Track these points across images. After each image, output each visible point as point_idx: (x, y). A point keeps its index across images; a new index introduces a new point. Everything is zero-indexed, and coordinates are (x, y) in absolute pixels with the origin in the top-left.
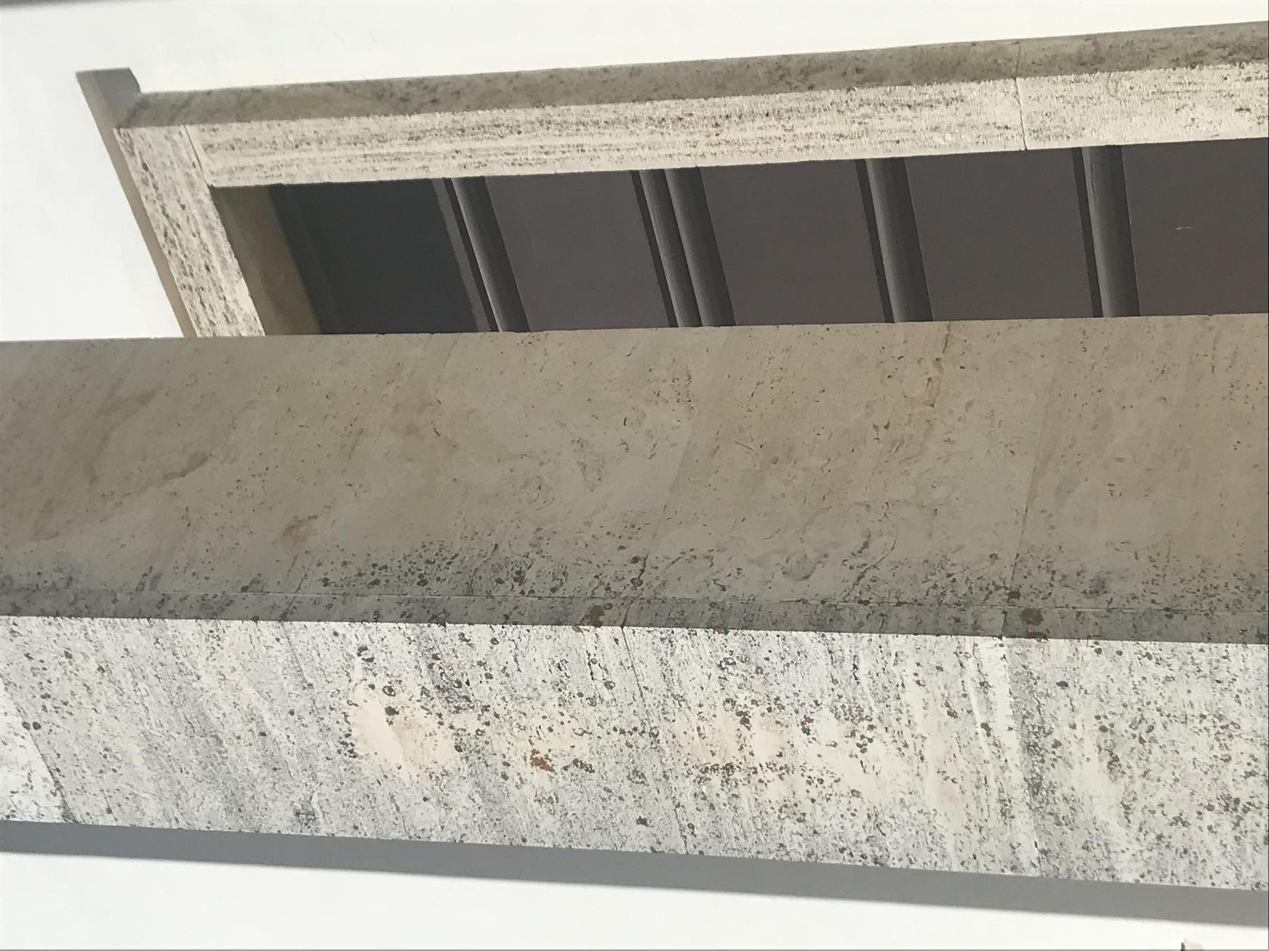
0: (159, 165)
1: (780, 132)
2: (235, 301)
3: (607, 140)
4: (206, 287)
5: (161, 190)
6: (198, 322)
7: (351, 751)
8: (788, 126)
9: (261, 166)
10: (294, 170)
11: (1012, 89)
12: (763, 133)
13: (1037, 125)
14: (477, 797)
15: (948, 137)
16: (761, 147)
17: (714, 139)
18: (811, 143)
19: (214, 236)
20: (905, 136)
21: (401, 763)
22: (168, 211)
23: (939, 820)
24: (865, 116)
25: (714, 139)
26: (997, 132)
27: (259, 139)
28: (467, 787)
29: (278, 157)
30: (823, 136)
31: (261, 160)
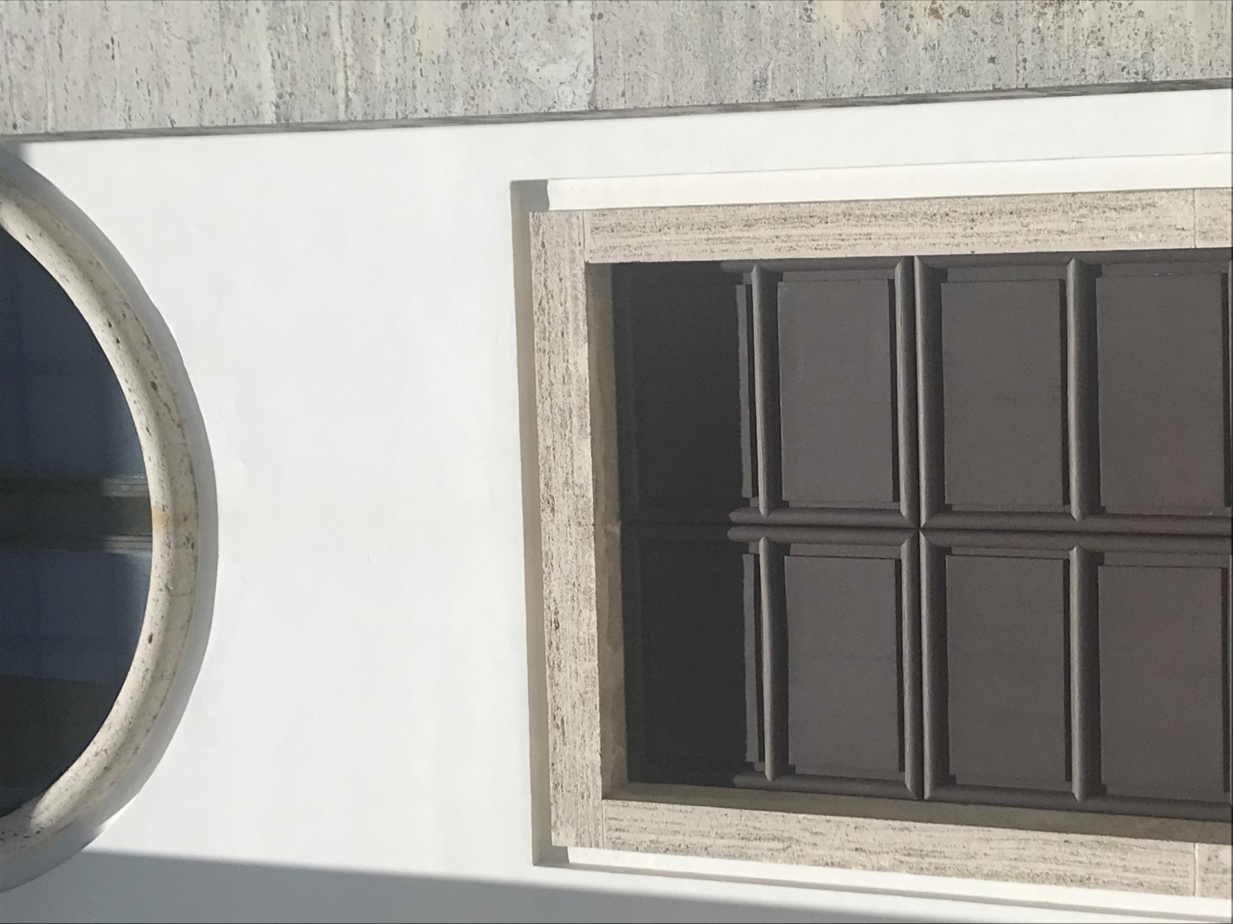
0: (554, 243)
1: (1018, 228)
2: (575, 363)
3: (890, 230)
4: (556, 351)
5: (548, 266)
6: (541, 382)
7: (809, 17)
8: (1025, 222)
9: (629, 246)
10: (652, 250)
11: (1190, 200)
12: (1005, 228)
13: (1206, 228)
14: (884, 51)
15: (1140, 235)
16: (1002, 239)
17: (969, 231)
18: (1040, 237)
19: (576, 306)
20: (1108, 233)
21: (840, 23)
22: (548, 283)
23: (1192, 32)
24: (1083, 216)
25: (969, 231)
26: (1177, 233)
27: (634, 223)
28: (880, 42)
29: (644, 239)
30: (1049, 232)
31: (630, 241)
